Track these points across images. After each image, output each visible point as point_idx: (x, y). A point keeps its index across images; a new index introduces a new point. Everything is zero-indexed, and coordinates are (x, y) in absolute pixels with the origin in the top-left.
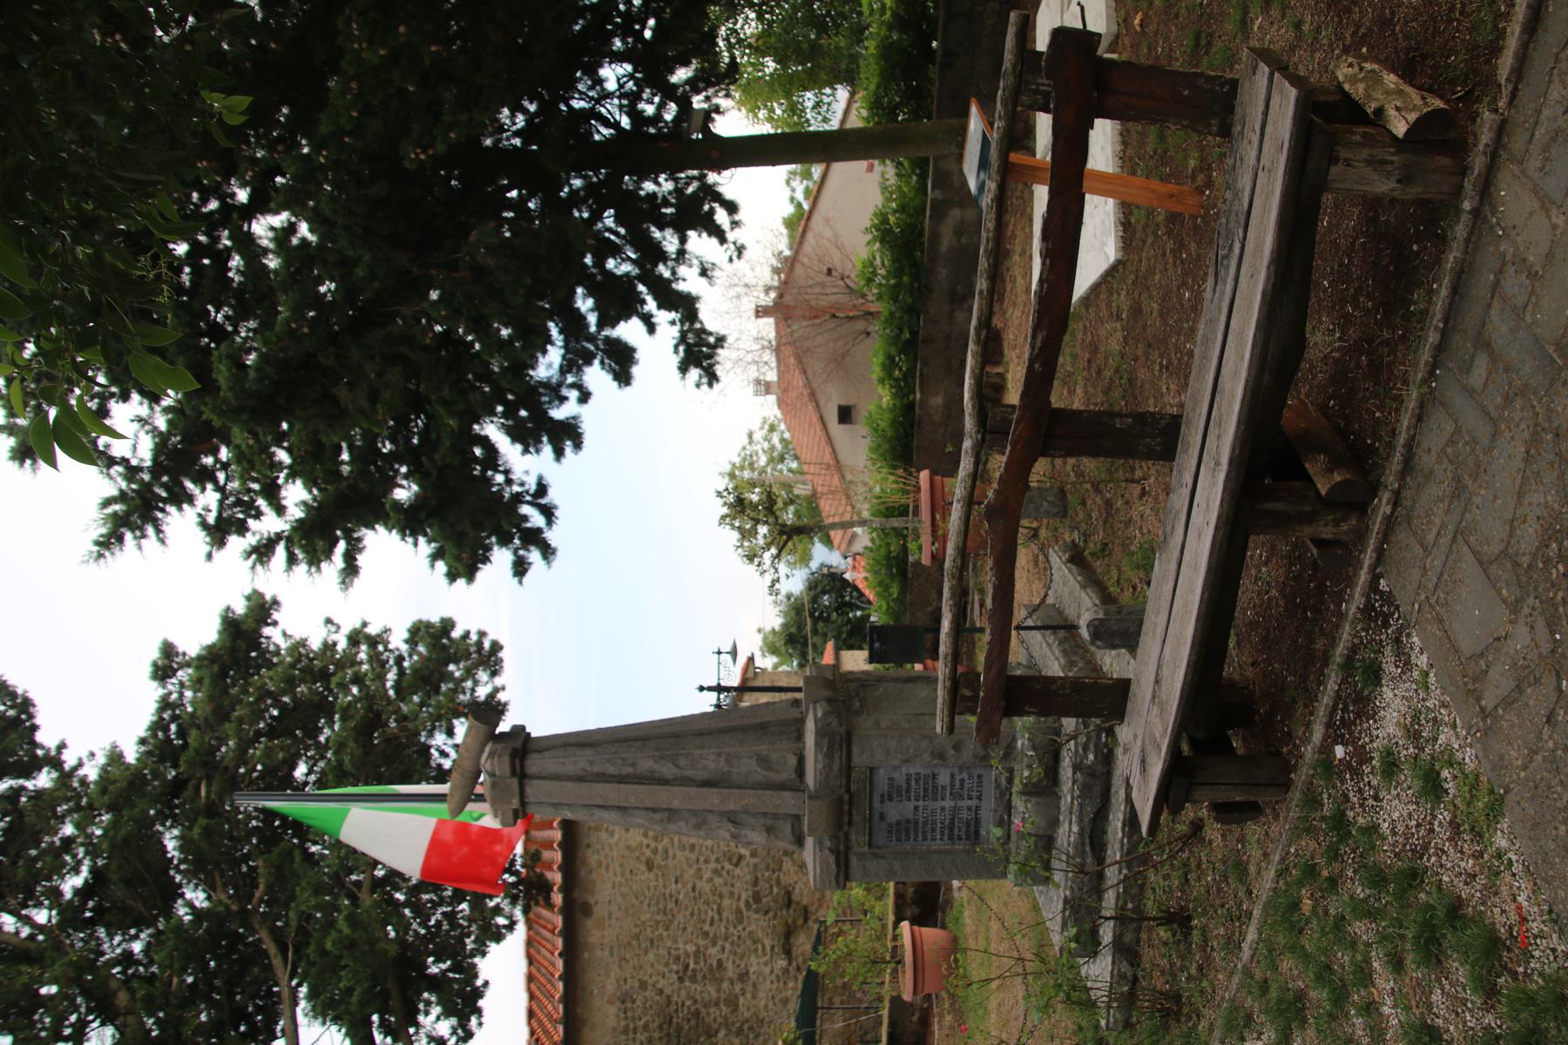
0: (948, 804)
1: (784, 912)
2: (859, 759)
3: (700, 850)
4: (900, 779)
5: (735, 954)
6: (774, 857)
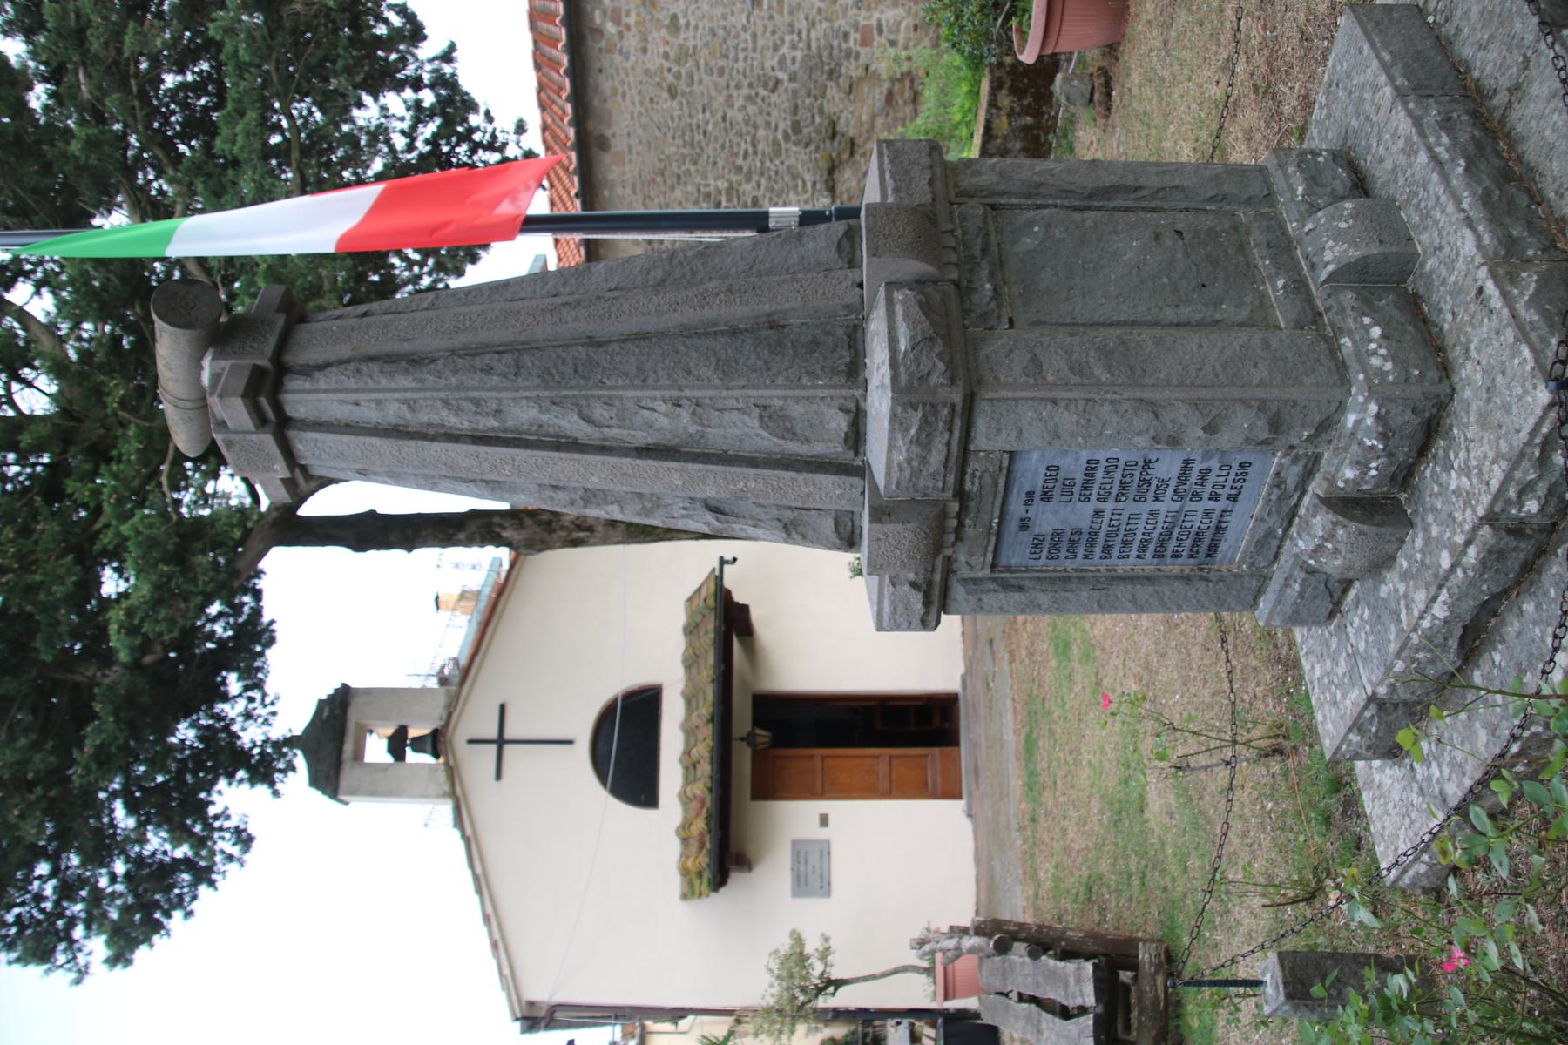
0: (1166, 506)
1: (828, 144)
2: (983, 438)
3: (731, 74)
4: (1073, 468)
5: (772, 190)
6: (816, 81)
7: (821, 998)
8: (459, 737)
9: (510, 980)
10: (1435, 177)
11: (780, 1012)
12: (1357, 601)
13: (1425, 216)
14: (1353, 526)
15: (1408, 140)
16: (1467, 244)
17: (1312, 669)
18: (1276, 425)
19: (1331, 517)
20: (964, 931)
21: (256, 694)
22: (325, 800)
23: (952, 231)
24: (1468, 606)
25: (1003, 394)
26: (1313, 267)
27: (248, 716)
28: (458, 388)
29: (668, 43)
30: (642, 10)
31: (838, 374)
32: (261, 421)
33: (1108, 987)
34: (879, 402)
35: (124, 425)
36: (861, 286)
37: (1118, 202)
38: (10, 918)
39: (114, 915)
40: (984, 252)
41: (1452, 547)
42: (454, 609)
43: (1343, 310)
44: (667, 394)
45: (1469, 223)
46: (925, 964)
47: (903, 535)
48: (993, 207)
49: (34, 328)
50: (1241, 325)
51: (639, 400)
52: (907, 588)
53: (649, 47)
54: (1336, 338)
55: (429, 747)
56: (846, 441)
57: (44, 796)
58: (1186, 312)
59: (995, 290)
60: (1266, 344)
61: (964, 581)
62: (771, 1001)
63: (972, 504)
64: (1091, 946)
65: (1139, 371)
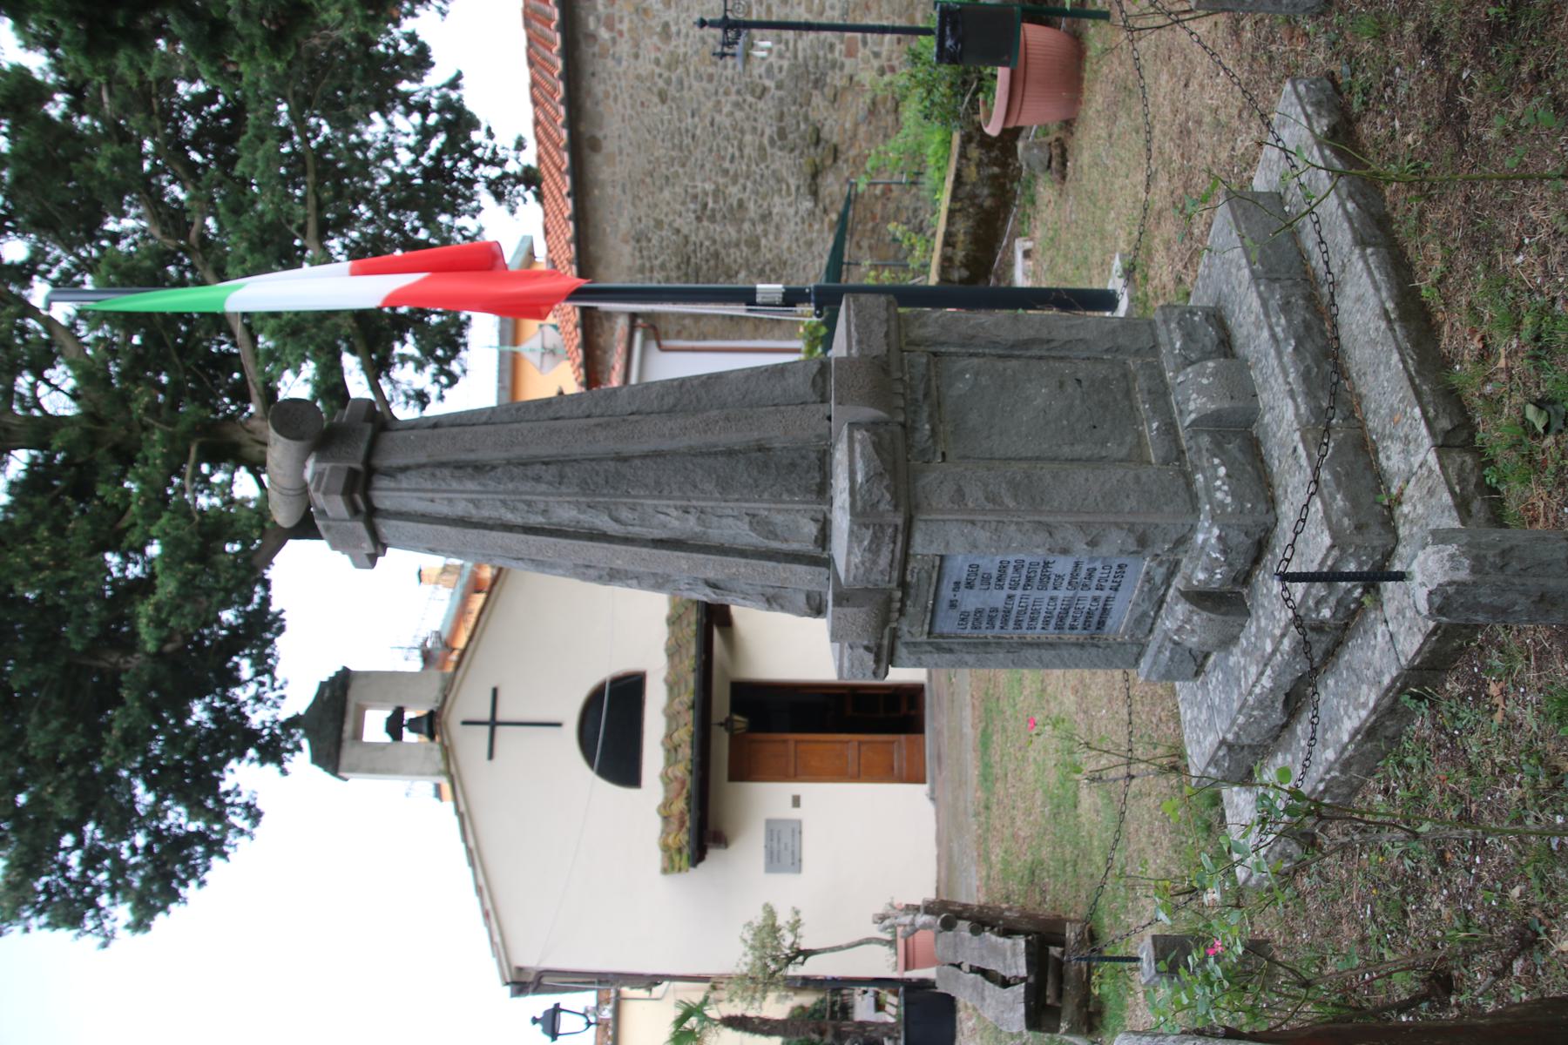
1: (812, 150)
2: (919, 545)
4: (990, 565)
5: (757, 193)
7: (791, 967)
8: (454, 718)
9: (501, 947)
10: (1272, 352)
11: (753, 979)
12: (1215, 666)
13: (1266, 381)
14: (1205, 615)
15: (1257, 317)
16: (1290, 413)
17: (1187, 714)
18: (1143, 542)
19: (1188, 606)
20: (916, 909)
21: (266, 678)
22: (327, 776)
23: (901, 379)
24: (1287, 681)
25: (933, 517)
26: (1181, 412)
27: (258, 699)
28: (514, 492)
29: (659, 49)
30: (634, 17)
31: (811, 492)
32: (355, 511)
33: (1037, 958)
34: (841, 521)
35: (146, 428)
36: (829, 418)
37: (1035, 352)
38: (39, 886)
39: (137, 883)
40: (926, 395)
41: (1273, 637)
42: (437, 583)
43: (1199, 450)
44: (679, 503)
45: (1292, 394)
46: (888, 937)
47: (859, 615)
48: (935, 354)
49: (58, 332)
50: (1122, 460)
51: (656, 506)
52: (862, 650)
53: (641, 53)
54: (1193, 473)
55: (425, 728)
56: (816, 541)
57: (74, 775)
58: (1079, 449)
59: (933, 430)
60: (1137, 479)
61: (907, 644)
62: (745, 969)
63: (912, 591)
64: (1025, 926)
65: (1038, 500)
